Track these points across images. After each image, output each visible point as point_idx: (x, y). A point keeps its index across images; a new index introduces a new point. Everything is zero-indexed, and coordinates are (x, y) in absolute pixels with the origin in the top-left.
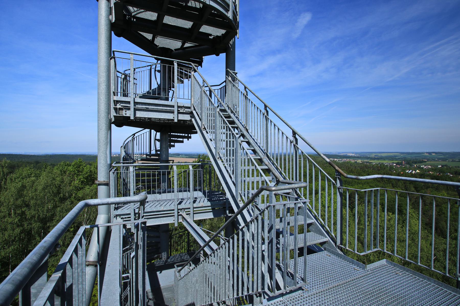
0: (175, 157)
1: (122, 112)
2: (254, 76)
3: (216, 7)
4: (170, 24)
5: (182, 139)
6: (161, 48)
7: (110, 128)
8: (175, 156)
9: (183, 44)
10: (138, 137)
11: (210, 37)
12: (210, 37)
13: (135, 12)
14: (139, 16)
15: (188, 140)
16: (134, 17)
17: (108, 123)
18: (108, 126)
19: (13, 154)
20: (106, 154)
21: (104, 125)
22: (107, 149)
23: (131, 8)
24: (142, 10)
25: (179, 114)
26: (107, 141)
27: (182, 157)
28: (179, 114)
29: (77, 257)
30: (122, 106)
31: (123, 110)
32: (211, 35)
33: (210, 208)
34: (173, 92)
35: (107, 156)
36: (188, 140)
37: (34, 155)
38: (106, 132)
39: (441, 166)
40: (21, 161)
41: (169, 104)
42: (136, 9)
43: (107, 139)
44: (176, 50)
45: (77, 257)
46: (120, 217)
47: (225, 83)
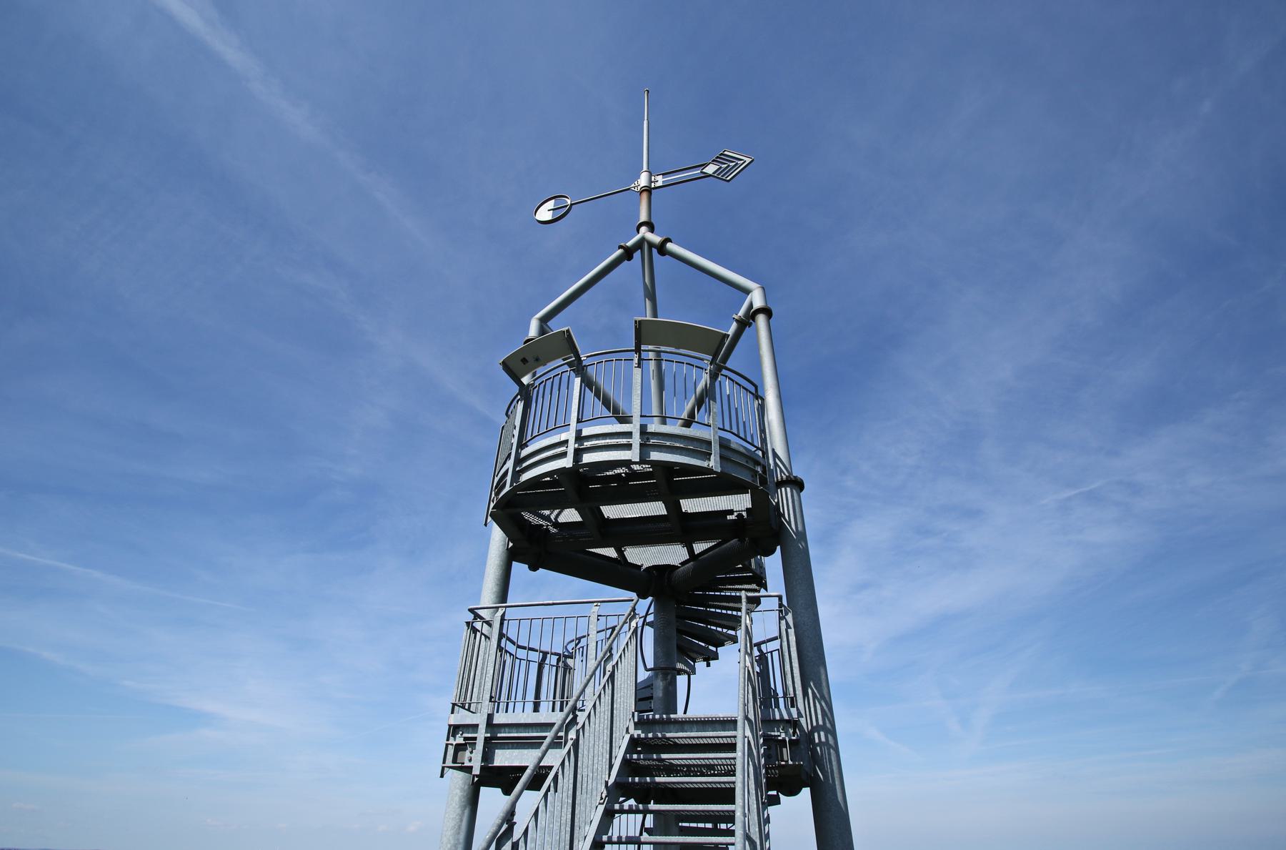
1: (463, 757)
6: (649, 569)
9: (691, 551)
10: (581, 649)
11: (729, 517)
12: (729, 517)
15: (708, 665)
17: (466, 787)
18: (465, 794)
21: (458, 791)
25: (515, 564)
26: (458, 840)
28: (515, 564)
29: (528, 826)
30: (465, 739)
32: (731, 512)
34: (648, 667)
36: (708, 665)
38: (459, 811)
43: (459, 833)
44: (683, 563)
45: (528, 826)
47: (483, 636)
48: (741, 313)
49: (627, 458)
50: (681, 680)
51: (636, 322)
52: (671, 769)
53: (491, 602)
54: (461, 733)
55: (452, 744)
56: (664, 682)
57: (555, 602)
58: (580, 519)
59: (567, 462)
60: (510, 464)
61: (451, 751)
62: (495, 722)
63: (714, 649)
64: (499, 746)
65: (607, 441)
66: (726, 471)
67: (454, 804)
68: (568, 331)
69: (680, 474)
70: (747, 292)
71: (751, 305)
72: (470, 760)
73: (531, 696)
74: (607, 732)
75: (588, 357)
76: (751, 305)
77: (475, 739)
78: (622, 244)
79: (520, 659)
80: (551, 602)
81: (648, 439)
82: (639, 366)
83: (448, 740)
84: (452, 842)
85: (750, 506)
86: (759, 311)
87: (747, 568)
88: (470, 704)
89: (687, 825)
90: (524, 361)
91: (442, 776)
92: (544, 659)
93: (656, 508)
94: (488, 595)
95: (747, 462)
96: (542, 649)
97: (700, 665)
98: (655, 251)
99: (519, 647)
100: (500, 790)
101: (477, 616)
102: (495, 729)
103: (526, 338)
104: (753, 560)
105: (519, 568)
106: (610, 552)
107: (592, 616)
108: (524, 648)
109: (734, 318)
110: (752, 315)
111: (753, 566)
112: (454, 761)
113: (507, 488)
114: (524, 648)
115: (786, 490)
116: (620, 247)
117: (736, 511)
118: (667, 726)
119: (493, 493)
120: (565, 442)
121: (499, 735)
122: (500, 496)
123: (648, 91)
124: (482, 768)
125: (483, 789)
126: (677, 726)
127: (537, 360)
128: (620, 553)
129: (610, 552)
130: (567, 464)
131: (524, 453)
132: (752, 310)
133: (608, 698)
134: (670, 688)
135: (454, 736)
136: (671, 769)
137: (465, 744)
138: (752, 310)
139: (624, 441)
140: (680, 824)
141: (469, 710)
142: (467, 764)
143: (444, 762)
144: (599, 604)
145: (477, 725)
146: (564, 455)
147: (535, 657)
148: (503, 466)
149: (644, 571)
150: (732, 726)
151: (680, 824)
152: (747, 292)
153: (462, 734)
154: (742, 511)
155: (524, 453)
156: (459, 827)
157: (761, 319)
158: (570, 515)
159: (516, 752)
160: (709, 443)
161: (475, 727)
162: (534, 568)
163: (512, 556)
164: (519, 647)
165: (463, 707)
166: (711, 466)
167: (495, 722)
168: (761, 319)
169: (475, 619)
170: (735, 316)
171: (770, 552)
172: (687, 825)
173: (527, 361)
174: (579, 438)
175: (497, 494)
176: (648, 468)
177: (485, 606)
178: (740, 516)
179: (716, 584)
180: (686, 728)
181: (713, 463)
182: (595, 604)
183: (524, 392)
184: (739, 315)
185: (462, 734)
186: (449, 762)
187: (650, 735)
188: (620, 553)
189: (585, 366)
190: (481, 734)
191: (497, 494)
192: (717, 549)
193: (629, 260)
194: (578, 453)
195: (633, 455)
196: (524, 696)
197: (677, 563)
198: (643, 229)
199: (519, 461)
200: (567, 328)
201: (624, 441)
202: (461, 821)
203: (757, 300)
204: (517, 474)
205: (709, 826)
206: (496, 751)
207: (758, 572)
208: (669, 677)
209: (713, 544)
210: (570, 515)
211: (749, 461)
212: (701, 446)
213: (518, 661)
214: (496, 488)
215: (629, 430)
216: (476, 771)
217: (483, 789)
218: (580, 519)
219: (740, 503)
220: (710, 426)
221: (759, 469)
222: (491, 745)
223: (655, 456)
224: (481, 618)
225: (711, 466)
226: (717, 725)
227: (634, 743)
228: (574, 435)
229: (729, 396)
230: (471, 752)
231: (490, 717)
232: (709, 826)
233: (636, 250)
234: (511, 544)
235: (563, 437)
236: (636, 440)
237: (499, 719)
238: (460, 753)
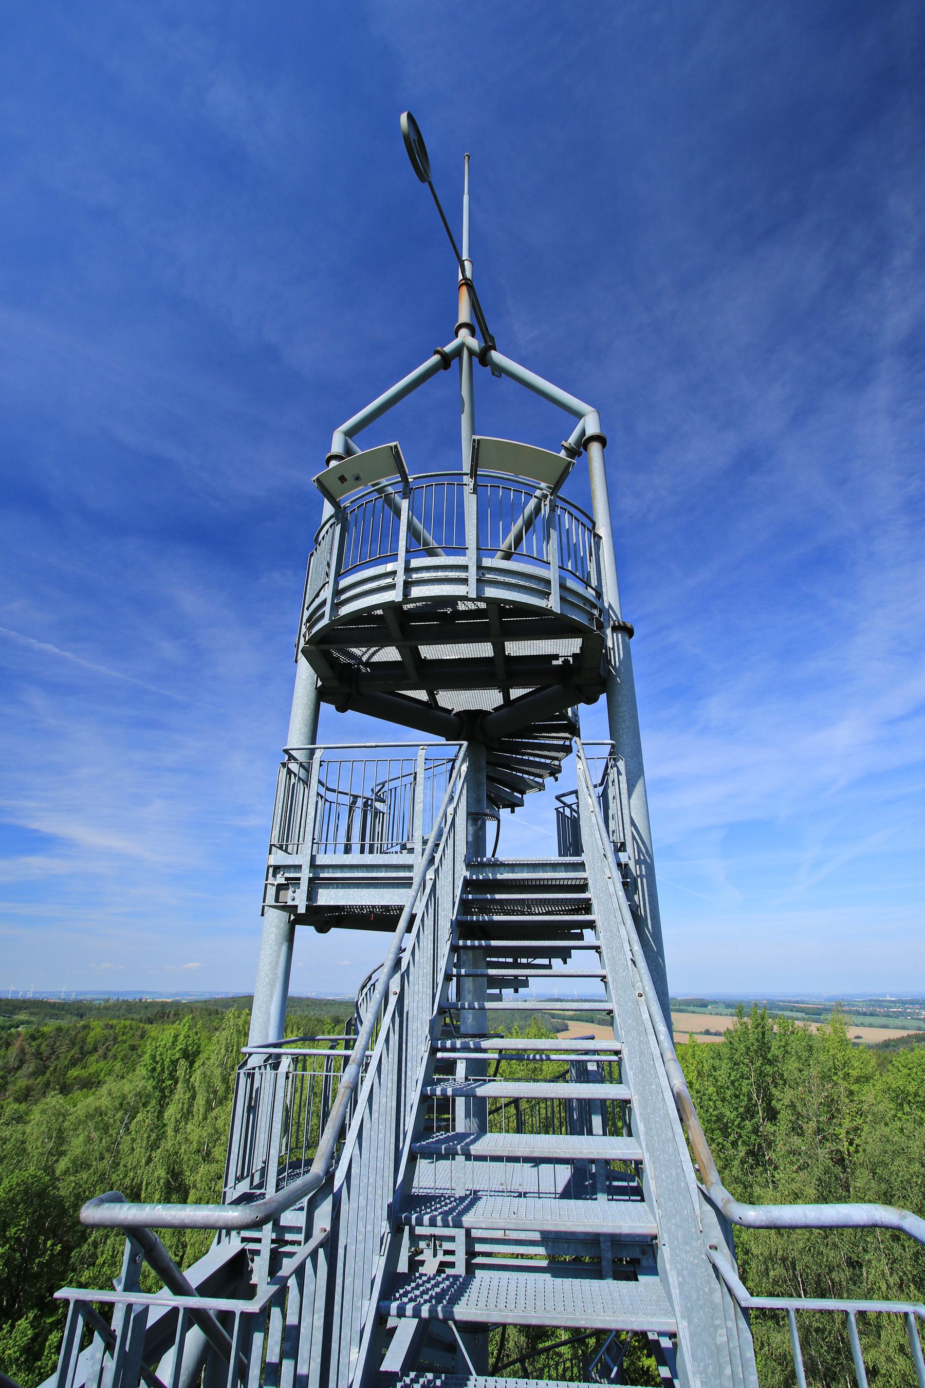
0: (694, 1012)
1: (286, 896)
2: (902, 718)
3: (523, 601)
4: (448, 658)
5: (545, 961)
6: (459, 714)
7: (290, 938)
8: (691, 1008)
9: (506, 696)
11: (554, 662)
12: (554, 662)
13: (364, 654)
14: (375, 659)
16: (368, 664)
17: (282, 925)
19: (296, 996)
20: (269, 1014)
21: (274, 929)
22: (271, 996)
23: (356, 651)
24: (375, 649)
26: (276, 974)
27: (717, 1014)
30: (287, 879)
31: (288, 889)
32: (556, 657)
33: (541, 1250)
35: (268, 1019)
37: (333, 1000)
38: (275, 948)
39: (594, 1171)
40: (307, 1016)
41: (401, 863)
42: (364, 649)
44: (496, 709)
46: (239, 1233)
48: (572, 440)
49: (390, 600)
50: (491, 825)
51: (474, 440)
52: (504, 907)
53: (308, 741)
54: (282, 873)
55: (273, 885)
56: (475, 827)
57: (378, 744)
58: (399, 658)
59: (395, 596)
60: (327, 593)
61: (272, 891)
62: (318, 862)
63: (520, 796)
64: (323, 886)
65: (447, 574)
66: (564, 613)
67: (270, 941)
68: (396, 447)
69: (510, 613)
70: (579, 416)
71: (583, 433)
72: (294, 899)
73: (342, 839)
74: (451, 872)
75: (415, 479)
76: (583, 433)
77: (299, 879)
78: (439, 349)
79: (331, 802)
80: (374, 744)
81: (483, 574)
82: (475, 491)
83: (267, 880)
84: (270, 976)
85: (578, 651)
86: (593, 438)
87: (564, 716)
88: (287, 846)
89: (493, 959)
90: (342, 479)
91: (263, 915)
92: (354, 802)
93: (485, 650)
94: (296, 738)
95: (584, 605)
96: (352, 793)
97: (504, 813)
98: (475, 360)
99: (328, 789)
100: (332, 929)
101: (291, 757)
102: (319, 870)
103: (329, 454)
104: (569, 710)
105: (327, 708)
106: (422, 695)
107: (419, 759)
108: (334, 791)
109: (563, 445)
110: (585, 442)
111: (570, 714)
112: (277, 900)
113: (325, 621)
114: (334, 791)
115: (617, 636)
116: (437, 352)
117: (562, 657)
118: (497, 868)
119: (303, 627)
120: (394, 573)
121: (322, 875)
122: (314, 630)
123: (469, 156)
124: (307, 906)
125: (297, 926)
126: (507, 868)
127: (357, 478)
128: (432, 696)
129: (422, 695)
130: (396, 597)
131: (343, 583)
132: (585, 438)
133: (452, 840)
134: (480, 833)
135: (274, 875)
136: (504, 907)
137: (287, 885)
138: (585, 438)
139: (388, 581)
140: (488, 959)
141: (286, 851)
142: (290, 903)
143: (264, 902)
144: (426, 747)
145: (300, 866)
146: (392, 587)
147: (347, 800)
148: (313, 601)
149: (455, 715)
150: (581, 868)
151: (488, 959)
152: (579, 416)
153: (283, 875)
154: (567, 656)
155: (343, 583)
156: (277, 962)
157: (595, 449)
158: (390, 654)
159: (341, 892)
160: (548, 582)
161: (298, 868)
162: (341, 709)
163: (322, 695)
164: (328, 789)
165: (281, 848)
166: (549, 606)
167: (318, 862)
168: (595, 449)
169: (289, 760)
170: (564, 443)
171: (591, 700)
172: (493, 959)
173: (339, 478)
174: (408, 570)
175: (310, 629)
176: (483, 605)
177: (295, 747)
178: (566, 662)
179: (531, 731)
180: (516, 871)
181: (553, 603)
182: (422, 747)
183: (340, 515)
184: (569, 441)
185: (283, 875)
186: (270, 900)
187: (474, 877)
188: (432, 696)
189: (412, 489)
190: (305, 875)
191: (310, 629)
192: (536, 695)
193: (445, 369)
194: (407, 585)
195: (470, 590)
196: (335, 839)
197: (489, 709)
198: (464, 333)
199: (337, 592)
200: (394, 443)
201: (388, 581)
202: (278, 956)
203: (591, 424)
204: (336, 606)
205: (510, 960)
206: (320, 890)
207: (573, 720)
208: (479, 823)
209: (531, 690)
210: (390, 654)
211: (587, 604)
212: (542, 587)
213: (328, 804)
214: (308, 621)
215: (464, 563)
216: (302, 910)
217: (297, 926)
218: (399, 658)
219: (569, 647)
220: (549, 564)
221: (596, 612)
222: (315, 884)
223: (491, 592)
224: (295, 759)
225: (549, 606)
226: (547, 868)
227: (467, 883)
228: (403, 566)
229: (568, 529)
230: (294, 892)
231: (313, 858)
232: (510, 960)
233: (454, 357)
234: (320, 683)
235: (390, 567)
236: (472, 574)
237: (321, 860)
238: (282, 893)
